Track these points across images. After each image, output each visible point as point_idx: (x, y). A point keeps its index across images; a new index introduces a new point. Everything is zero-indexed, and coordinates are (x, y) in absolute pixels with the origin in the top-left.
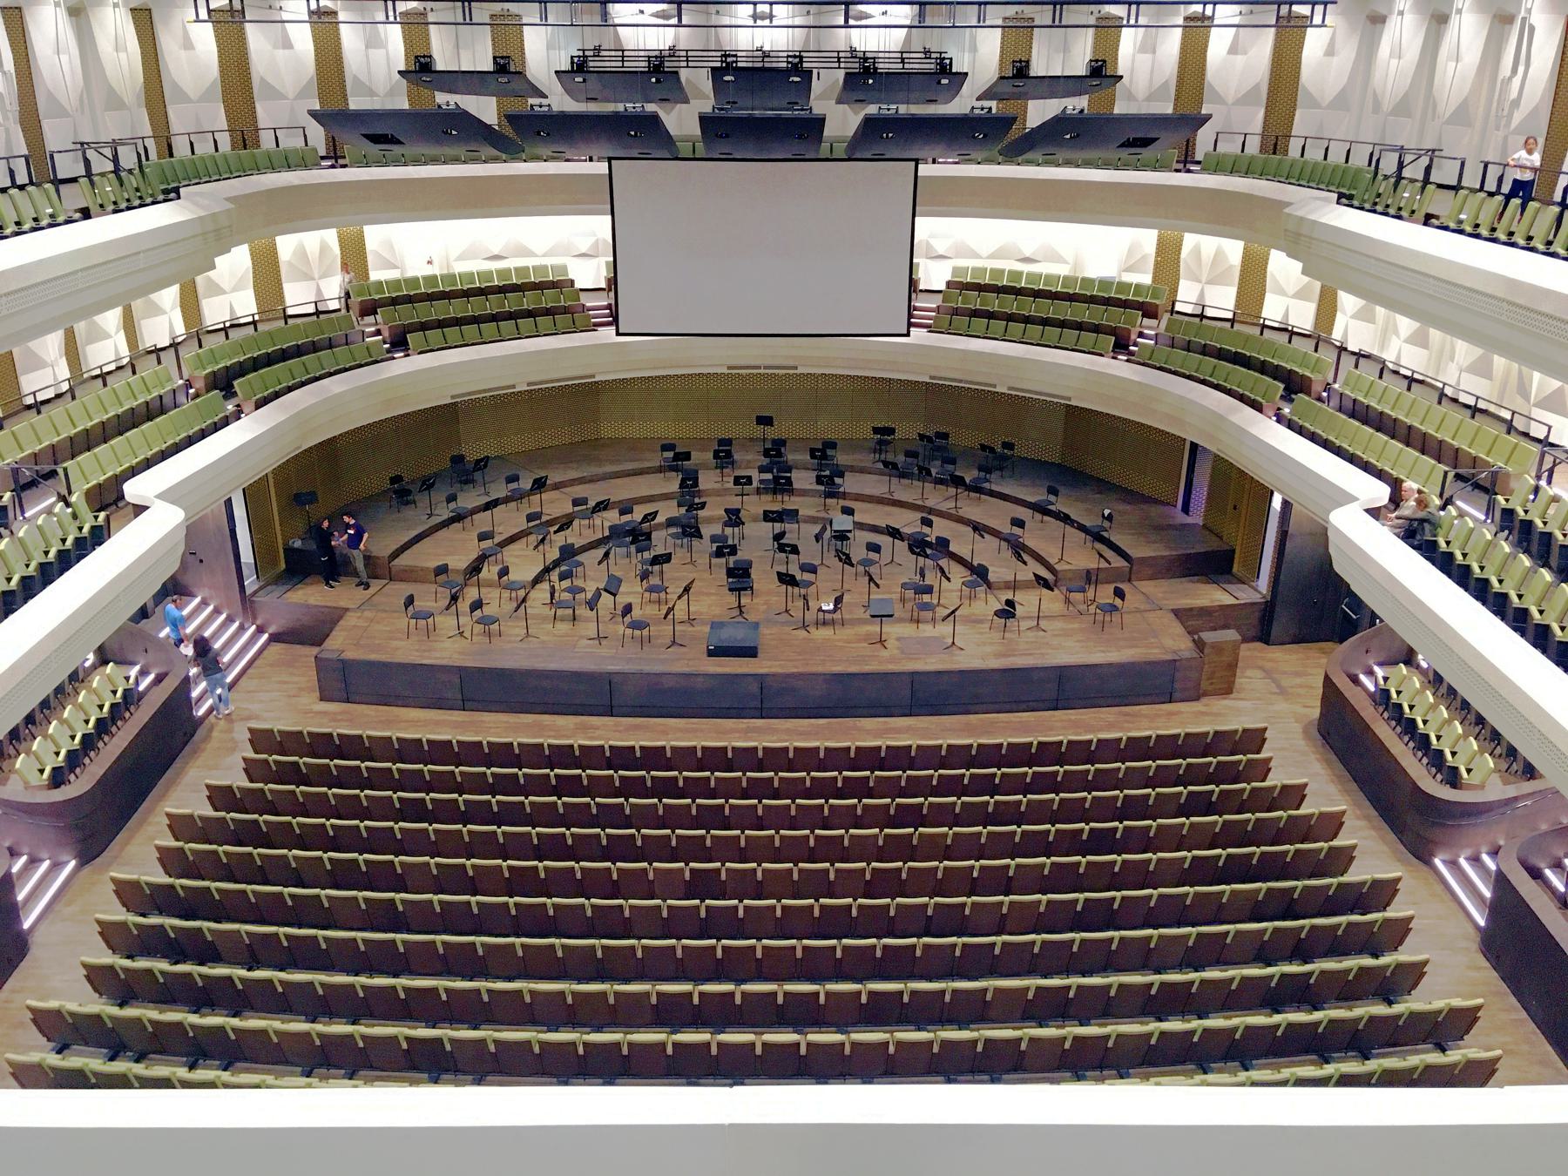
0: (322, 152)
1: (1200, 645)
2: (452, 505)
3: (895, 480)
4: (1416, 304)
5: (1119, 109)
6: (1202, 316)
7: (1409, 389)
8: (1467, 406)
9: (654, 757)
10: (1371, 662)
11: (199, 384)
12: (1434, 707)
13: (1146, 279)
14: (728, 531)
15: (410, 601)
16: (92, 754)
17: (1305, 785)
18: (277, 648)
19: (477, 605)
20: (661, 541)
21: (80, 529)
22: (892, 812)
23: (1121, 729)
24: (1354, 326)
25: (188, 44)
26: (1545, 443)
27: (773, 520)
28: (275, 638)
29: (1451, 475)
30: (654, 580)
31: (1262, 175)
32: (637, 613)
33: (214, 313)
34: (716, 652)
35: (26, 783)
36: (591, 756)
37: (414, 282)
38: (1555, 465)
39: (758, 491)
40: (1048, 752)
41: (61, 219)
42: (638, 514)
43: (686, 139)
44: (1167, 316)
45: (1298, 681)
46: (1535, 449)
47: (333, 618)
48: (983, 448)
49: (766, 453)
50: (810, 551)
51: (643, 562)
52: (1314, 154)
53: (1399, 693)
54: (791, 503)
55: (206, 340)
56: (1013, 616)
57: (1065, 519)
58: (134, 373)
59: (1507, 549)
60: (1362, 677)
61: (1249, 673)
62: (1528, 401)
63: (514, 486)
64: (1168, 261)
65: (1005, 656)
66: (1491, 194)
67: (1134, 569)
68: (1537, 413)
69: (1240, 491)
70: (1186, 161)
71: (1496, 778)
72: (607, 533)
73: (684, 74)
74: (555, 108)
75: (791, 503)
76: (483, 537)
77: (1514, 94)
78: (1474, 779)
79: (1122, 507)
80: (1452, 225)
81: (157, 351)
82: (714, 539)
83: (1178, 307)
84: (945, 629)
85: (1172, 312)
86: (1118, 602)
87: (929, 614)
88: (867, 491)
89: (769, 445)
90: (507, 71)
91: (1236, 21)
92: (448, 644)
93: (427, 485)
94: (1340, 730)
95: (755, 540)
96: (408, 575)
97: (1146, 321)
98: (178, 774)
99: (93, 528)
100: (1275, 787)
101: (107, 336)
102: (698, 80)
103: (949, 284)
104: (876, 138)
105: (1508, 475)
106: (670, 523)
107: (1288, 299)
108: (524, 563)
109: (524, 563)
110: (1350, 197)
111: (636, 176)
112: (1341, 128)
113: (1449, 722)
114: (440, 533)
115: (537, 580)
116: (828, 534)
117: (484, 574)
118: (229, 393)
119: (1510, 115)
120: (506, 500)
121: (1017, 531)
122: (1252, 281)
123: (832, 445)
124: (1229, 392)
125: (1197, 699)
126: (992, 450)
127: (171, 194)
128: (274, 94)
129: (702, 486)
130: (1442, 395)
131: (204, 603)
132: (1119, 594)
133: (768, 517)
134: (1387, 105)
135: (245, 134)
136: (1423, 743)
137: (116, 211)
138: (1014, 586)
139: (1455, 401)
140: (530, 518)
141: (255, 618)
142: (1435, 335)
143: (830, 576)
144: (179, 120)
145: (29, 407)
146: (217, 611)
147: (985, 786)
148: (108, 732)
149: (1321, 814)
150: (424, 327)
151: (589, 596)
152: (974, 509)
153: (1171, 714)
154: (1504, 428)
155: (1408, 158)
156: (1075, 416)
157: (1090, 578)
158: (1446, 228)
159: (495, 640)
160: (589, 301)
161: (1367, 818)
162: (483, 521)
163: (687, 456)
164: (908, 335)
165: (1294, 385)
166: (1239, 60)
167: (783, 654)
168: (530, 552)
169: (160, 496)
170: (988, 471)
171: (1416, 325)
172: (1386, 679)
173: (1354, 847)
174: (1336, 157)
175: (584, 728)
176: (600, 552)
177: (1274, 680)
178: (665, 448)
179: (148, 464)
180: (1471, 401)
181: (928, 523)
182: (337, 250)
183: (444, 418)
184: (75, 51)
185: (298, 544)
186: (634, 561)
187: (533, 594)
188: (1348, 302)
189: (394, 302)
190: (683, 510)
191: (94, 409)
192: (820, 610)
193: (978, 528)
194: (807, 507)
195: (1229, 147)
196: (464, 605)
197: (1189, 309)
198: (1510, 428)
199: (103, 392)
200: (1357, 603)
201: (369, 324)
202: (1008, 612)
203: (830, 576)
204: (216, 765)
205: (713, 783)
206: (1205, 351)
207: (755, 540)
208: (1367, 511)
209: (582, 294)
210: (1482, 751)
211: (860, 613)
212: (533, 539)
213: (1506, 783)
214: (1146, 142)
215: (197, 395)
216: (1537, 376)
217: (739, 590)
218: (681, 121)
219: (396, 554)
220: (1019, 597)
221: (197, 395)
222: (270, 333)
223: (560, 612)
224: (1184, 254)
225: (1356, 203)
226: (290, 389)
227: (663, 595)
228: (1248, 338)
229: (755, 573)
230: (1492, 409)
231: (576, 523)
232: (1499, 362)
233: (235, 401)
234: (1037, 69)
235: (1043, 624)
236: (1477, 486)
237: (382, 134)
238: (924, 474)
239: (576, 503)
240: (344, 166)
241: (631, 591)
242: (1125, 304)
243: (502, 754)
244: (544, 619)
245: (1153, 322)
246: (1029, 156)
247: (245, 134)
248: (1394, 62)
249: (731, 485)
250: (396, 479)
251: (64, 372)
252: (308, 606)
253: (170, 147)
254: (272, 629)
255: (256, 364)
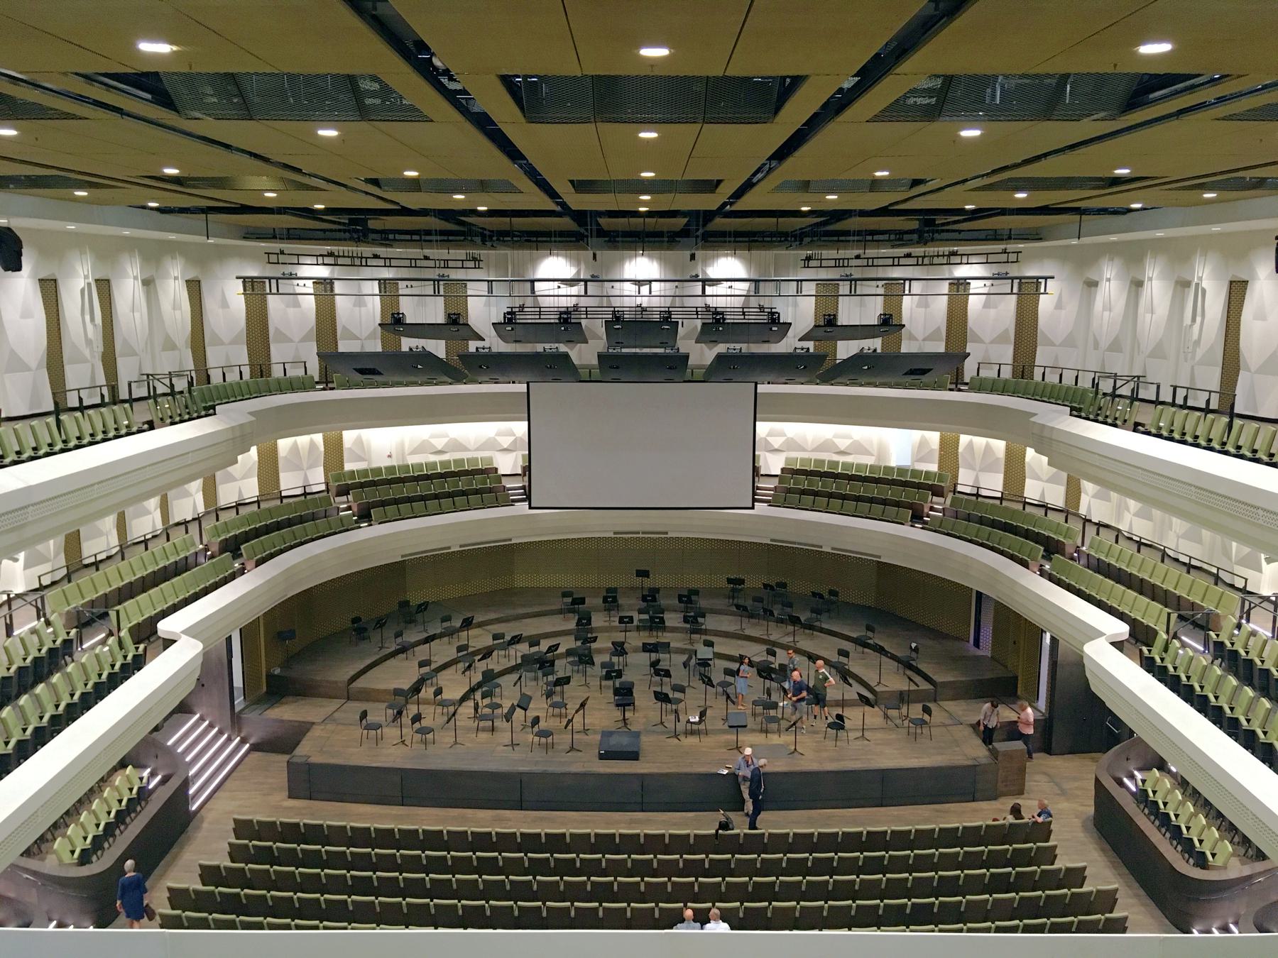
0: (317, 379)
1: (994, 754)
2: (399, 640)
3: (745, 620)
4: (1135, 484)
5: (905, 348)
6: (977, 495)
7: (1139, 551)
8: (1184, 564)
9: (556, 843)
10: (1131, 768)
11: (215, 548)
12: (1182, 803)
13: (933, 467)
14: (615, 659)
15: (364, 715)
16: (111, 840)
17: (1084, 868)
18: (256, 755)
19: (417, 718)
20: (562, 667)
21: (125, 657)
22: (750, 889)
23: (935, 823)
24: (1092, 503)
25: (225, 304)
26: (1244, 591)
27: (650, 651)
28: (254, 748)
29: (1174, 616)
30: (557, 699)
31: (1014, 393)
32: (543, 724)
33: (227, 496)
34: (607, 756)
35: (60, 860)
36: (506, 842)
37: (378, 471)
38: (1250, 609)
39: (638, 628)
40: (876, 840)
41: (134, 429)
42: (544, 645)
43: (584, 367)
44: (950, 495)
45: (1076, 784)
46: (1237, 596)
47: (301, 730)
48: (814, 594)
49: (644, 599)
50: (679, 676)
51: (547, 684)
52: (1052, 378)
53: (1154, 792)
54: (664, 637)
55: (221, 514)
56: (842, 728)
57: (880, 650)
58: (168, 540)
59: (1219, 672)
60: (1126, 780)
61: (1038, 777)
62: (1230, 559)
63: (446, 624)
64: (949, 452)
65: (838, 760)
66: (1181, 407)
67: (937, 693)
68: (1239, 570)
69: (1019, 631)
70: (957, 383)
71: (1235, 862)
72: (519, 661)
73: (584, 322)
74: (494, 350)
75: (664, 637)
76: (422, 664)
77: (1195, 337)
78: (1219, 861)
79: (930, 643)
80: (1153, 431)
81: (185, 523)
82: (603, 665)
83: (960, 488)
84: (787, 738)
85: (955, 491)
86: (926, 717)
87: (774, 726)
88: (724, 628)
89: (646, 593)
90: (456, 323)
91: (985, 290)
92: (392, 750)
93: (380, 624)
94: (1110, 824)
95: (636, 667)
96: (368, 696)
97: (935, 499)
98: (175, 858)
99: (134, 656)
100: (1060, 870)
101: (149, 513)
102: (595, 327)
103: (783, 470)
104: (725, 368)
105: (1217, 615)
106: (569, 653)
107: (1044, 485)
108: (454, 685)
109: (454, 685)
110: (1080, 410)
111: (547, 392)
112: (1070, 360)
113: (1195, 815)
114: (368, 674)
115: (464, 699)
116: (693, 661)
117: (422, 694)
118: (236, 554)
119: (1194, 352)
120: (441, 636)
121: (843, 660)
122: (1015, 470)
123: (696, 592)
124: (1002, 553)
125: (995, 799)
126: (821, 596)
127: (209, 411)
128: (285, 339)
129: (594, 624)
130: (1164, 556)
131: (202, 719)
132: (927, 710)
133: (647, 648)
134: (1104, 343)
135: (261, 366)
136: (1176, 833)
137: (173, 423)
138: (843, 703)
139: (1177, 560)
140: (460, 649)
141: (240, 731)
142: (1157, 513)
143: (695, 696)
144: (214, 358)
145: (87, 566)
146: (211, 726)
147: (824, 867)
148: (123, 822)
149: (1098, 891)
150: (383, 504)
151: (505, 711)
152: (806, 644)
153: (975, 810)
154: (1212, 580)
155: (1119, 383)
156: (886, 571)
157: (903, 698)
158: (1148, 433)
159: (430, 747)
160: (509, 483)
161: (1137, 896)
162: (422, 652)
163: (582, 601)
164: (753, 508)
165: (1052, 548)
166: (992, 312)
167: (662, 756)
168: (459, 676)
169: (184, 632)
170: (818, 612)
171: (1139, 505)
172: (1144, 781)
173: (1126, 918)
174: (1068, 380)
175: (500, 820)
176: (515, 676)
177: (1057, 784)
178: (565, 595)
179: (175, 608)
180: (1186, 560)
181: (774, 654)
182: (322, 449)
183: (393, 574)
184: (145, 310)
185: (277, 671)
186: (541, 683)
187: (461, 710)
188: (1088, 487)
189: (362, 485)
190: (579, 643)
191: (138, 566)
192: (688, 721)
193: (812, 658)
194: (676, 641)
195: (989, 373)
196: (406, 720)
197: (968, 490)
198: (1217, 579)
199: (145, 555)
200: (1117, 721)
201: (342, 502)
202: (838, 724)
203: (695, 696)
204: (209, 846)
205: (604, 864)
206: (981, 521)
207: (636, 667)
208: (1113, 644)
209: (504, 480)
210: (1222, 838)
211: (720, 725)
212: (461, 666)
213: (1243, 864)
214: (924, 372)
215: (212, 557)
216: (1234, 544)
217: (624, 705)
218: (584, 354)
219: (354, 678)
220: (847, 713)
221: (212, 557)
222: (269, 510)
223: (482, 724)
224: (960, 450)
225: (1083, 414)
226: (282, 552)
227: (563, 710)
228: (1015, 511)
229: (636, 693)
230: (1205, 566)
231: (495, 653)
232: (1206, 534)
233: (241, 560)
234: (843, 320)
235: (866, 734)
236: (1196, 625)
237: (367, 369)
238: (768, 613)
239: (495, 637)
240: (332, 389)
241: (539, 706)
242: (919, 486)
243: (434, 839)
244: (469, 730)
245: (941, 500)
246: (839, 380)
247: (261, 366)
248: (1106, 314)
249: (617, 624)
250: (356, 620)
251: (114, 541)
252: (282, 721)
253: (208, 376)
254: (252, 741)
255: (257, 533)
